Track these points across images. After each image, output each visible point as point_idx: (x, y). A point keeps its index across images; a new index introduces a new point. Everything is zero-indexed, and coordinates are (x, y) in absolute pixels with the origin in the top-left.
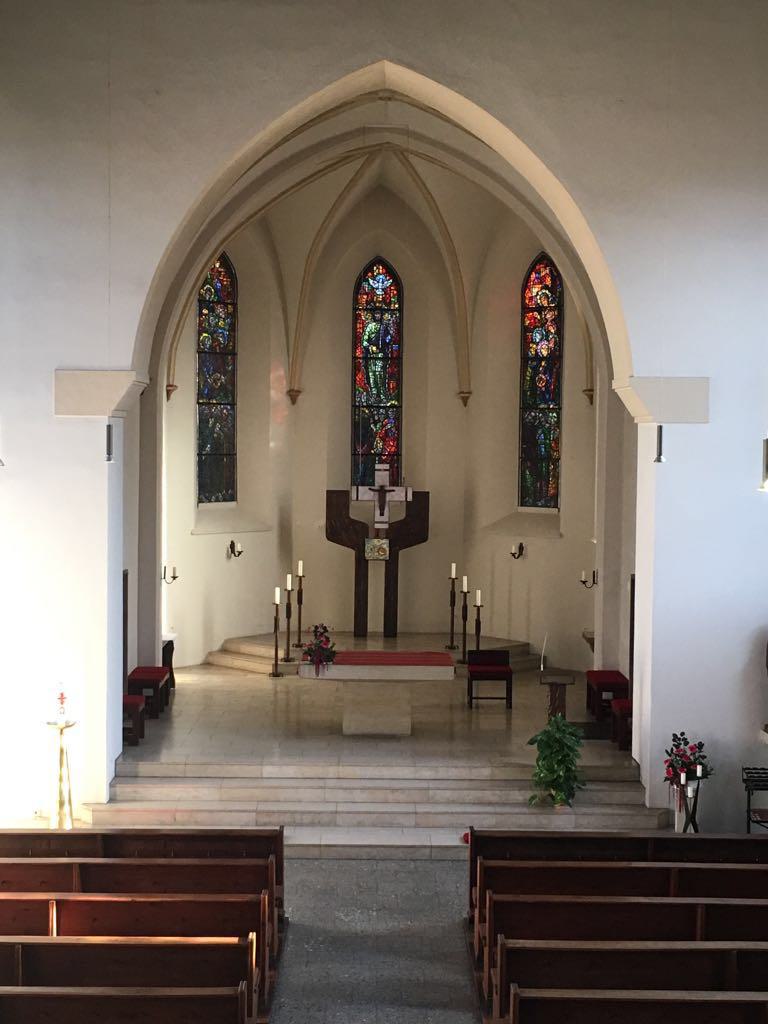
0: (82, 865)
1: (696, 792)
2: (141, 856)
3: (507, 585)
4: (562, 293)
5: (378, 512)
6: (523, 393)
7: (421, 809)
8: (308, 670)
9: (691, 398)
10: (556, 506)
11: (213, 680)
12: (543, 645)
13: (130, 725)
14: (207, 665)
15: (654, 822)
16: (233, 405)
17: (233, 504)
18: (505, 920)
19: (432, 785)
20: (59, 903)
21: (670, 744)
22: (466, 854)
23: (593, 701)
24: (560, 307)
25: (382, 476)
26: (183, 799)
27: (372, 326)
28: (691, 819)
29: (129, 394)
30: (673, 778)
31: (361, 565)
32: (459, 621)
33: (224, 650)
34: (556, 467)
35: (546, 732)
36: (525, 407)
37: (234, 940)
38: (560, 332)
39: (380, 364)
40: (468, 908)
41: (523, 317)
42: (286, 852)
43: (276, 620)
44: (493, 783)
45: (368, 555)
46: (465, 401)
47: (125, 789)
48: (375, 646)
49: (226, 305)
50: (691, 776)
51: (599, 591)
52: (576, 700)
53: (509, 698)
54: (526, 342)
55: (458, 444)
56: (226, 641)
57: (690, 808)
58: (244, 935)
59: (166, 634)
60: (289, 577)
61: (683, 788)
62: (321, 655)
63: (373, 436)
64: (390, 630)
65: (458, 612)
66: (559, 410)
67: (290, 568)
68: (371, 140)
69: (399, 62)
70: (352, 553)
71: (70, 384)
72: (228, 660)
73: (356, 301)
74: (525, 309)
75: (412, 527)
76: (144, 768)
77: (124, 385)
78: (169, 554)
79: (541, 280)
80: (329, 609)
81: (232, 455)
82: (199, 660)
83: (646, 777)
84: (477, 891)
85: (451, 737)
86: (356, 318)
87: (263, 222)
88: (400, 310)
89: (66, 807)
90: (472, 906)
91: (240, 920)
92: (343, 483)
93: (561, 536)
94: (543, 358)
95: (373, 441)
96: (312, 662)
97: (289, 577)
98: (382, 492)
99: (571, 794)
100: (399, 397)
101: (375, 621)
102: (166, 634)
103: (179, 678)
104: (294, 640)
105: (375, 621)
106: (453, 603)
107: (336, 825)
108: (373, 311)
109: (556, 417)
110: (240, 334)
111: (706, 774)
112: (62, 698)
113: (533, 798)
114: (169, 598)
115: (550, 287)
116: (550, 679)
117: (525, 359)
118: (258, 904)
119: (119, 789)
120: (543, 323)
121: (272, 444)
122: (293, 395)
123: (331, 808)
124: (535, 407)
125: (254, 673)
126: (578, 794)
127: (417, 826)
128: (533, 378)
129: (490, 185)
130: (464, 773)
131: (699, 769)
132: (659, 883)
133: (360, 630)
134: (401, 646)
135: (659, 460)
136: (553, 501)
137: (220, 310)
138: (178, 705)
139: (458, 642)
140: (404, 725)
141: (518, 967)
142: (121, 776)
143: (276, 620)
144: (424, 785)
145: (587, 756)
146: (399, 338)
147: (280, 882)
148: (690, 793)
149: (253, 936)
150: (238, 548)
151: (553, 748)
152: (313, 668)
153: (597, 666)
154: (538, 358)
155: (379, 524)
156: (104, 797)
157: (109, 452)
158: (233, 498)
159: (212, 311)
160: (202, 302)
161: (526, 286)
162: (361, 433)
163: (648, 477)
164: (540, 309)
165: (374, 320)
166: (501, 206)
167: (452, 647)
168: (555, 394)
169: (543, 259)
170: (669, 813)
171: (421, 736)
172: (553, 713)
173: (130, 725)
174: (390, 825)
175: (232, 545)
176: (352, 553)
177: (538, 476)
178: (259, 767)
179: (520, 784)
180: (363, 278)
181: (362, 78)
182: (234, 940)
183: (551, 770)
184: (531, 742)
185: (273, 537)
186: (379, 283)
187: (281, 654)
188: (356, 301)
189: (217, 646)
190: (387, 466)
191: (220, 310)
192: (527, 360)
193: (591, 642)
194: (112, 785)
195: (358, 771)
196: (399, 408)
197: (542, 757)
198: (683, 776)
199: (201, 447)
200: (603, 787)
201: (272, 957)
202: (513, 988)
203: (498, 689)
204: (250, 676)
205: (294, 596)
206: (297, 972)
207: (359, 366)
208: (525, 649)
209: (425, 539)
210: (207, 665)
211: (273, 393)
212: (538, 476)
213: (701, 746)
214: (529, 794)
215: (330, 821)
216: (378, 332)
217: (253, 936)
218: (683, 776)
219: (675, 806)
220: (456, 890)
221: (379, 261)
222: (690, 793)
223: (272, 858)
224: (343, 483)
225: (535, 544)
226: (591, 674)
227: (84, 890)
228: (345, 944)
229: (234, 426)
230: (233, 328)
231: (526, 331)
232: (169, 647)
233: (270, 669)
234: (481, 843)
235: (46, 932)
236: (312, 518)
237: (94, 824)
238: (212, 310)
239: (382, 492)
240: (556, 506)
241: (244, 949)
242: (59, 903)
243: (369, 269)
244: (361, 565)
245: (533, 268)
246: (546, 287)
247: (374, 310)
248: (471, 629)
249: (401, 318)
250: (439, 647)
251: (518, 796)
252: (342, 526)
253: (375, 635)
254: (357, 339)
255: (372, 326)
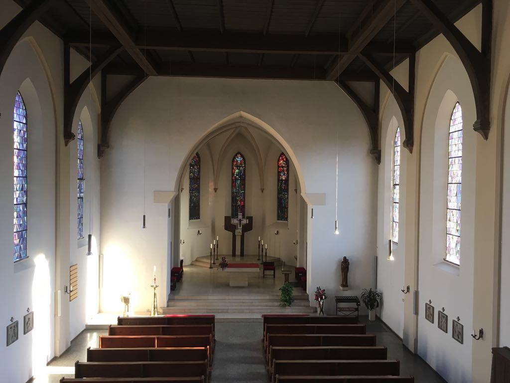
0: (163, 327)
1: (323, 303)
2: (178, 324)
3: (274, 243)
4: (288, 163)
5: (239, 226)
6: (278, 190)
7: (250, 308)
8: (221, 269)
9: (321, 199)
10: (287, 220)
11: (194, 269)
12: (283, 259)
13: (172, 284)
14: (192, 265)
15: (312, 311)
16: (199, 193)
17: (198, 220)
18: (272, 341)
19: (254, 301)
20: (158, 338)
21: (316, 290)
22: (263, 321)
23: (297, 275)
24: (288, 167)
25: (240, 217)
26: (187, 307)
27: (237, 171)
28: (322, 310)
29: (173, 198)
30: (317, 299)
31: (234, 237)
32: (261, 251)
33: (196, 261)
34: (287, 210)
35: (283, 287)
36: (279, 193)
37: (203, 348)
38: (288, 173)
39: (239, 181)
40: (263, 336)
41: (278, 168)
42: (216, 321)
43: (211, 253)
44: (270, 300)
45: (236, 234)
46: (262, 191)
47: (172, 303)
48: (238, 260)
49: (197, 165)
50: (322, 299)
51: (298, 246)
52: (292, 278)
53: (274, 275)
54: (279, 175)
55: (261, 203)
56: (198, 258)
57: (321, 307)
58: (206, 347)
59: (181, 258)
60: (215, 241)
61: (319, 302)
62: (224, 265)
63: (237, 201)
64: (242, 254)
65: (261, 249)
66: (288, 195)
67: (214, 238)
68: (237, 125)
69: (243, 111)
70: (232, 233)
71: (158, 195)
72: (197, 263)
73: (233, 164)
74: (279, 167)
75: (248, 228)
76: (176, 297)
77: (172, 196)
78: (183, 236)
79: (283, 159)
80: (225, 249)
81: (199, 204)
82: (190, 263)
83: (310, 299)
84: (265, 333)
85: (259, 287)
86: (233, 169)
87: (209, 145)
88: (245, 166)
89: (156, 309)
90: (264, 336)
91: (205, 342)
92: (230, 215)
93: (288, 229)
94: (284, 180)
95: (238, 205)
96: (221, 267)
97: (215, 241)
98: (240, 221)
99: (290, 303)
100: (244, 190)
101: (238, 252)
102: (181, 258)
103: (185, 269)
104: (216, 258)
105: (238, 252)
106: (259, 248)
107: (228, 313)
108: (237, 167)
109: (286, 198)
110: (202, 174)
111: (325, 298)
112: (155, 279)
113: (280, 305)
114: (183, 248)
115: (285, 166)
116: (285, 272)
117: (279, 180)
118: (209, 337)
119: (170, 303)
120: (283, 171)
121: (210, 203)
122: (216, 190)
123: (227, 308)
124: (281, 193)
125: (205, 268)
126: (292, 303)
127: (250, 312)
128: (281, 186)
129: (269, 137)
130: (262, 298)
131: (324, 297)
132: (312, 330)
133: (234, 255)
134: (247, 261)
135: (312, 209)
136: (286, 219)
137: (195, 167)
138: (184, 278)
139: (261, 258)
140: (246, 284)
141: (276, 354)
142: (171, 299)
143: (211, 253)
144: (251, 301)
145: (295, 292)
146: (244, 174)
147: (214, 330)
148: (321, 303)
149: (208, 347)
150: (200, 232)
151: (286, 291)
152: (222, 269)
153: (298, 266)
154: (282, 180)
155: (239, 222)
156: (166, 306)
157: (169, 216)
158: (199, 218)
159: (195, 171)
160: (191, 165)
161: (279, 161)
162: (234, 200)
163: (310, 222)
164: (283, 167)
165: (238, 169)
166: (271, 142)
167: (259, 260)
168: (287, 190)
169: (283, 154)
170: (316, 308)
171: (251, 287)
172: (285, 282)
173: (172, 284)
174: (243, 312)
175: (199, 232)
176: (231, 234)
177: (282, 212)
178: (217, 327)
179: (276, 300)
180: (234, 158)
181: (237, 114)
182: (203, 348)
183: (285, 297)
184: (280, 290)
185: (210, 229)
186: (239, 159)
187: (212, 262)
188: (233, 164)
189: (194, 260)
190: (241, 214)
191: (195, 167)
192: (279, 180)
193: (296, 259)
194: (168, 302)
195: (234, 297)
196: (245, 193)
197: (283, 293)
198: (319, 299)
199: (190, 205)
200: (298, 301)
201: (213, 351)
202: (274, 360)
203: (272, 272)
204: (204, 268)
205: (216, 246)
206: (219, 355)
207: (233, 182)
208: (279, 260)
209: (251, 229)
210: (192, 265)
211: (210, 190)
212: (282, 212)
213: (324, 290)
214: (279, 303)
215: (227, 311)
216: (239, 172)
217: (208, 347)
218: (319, 299)
219: (318, 306)
220: (260, 332)
221: (239, 153)
222: (321, 303)
223: (212, 325)
224: (230, 215)
225: (281, 231)
226: (297, 269)
227: (163, 335)
228: (231, 347)
229: (199, 199)
230: (199, 172)
231: (279, 173)
232: (182, 261)
233: (209, 266)
234: (267, 319)
235: (154, 347)
236: (221, 224)
237: (164, 313)
238: (193, 167)
239: (240, 221)
240: (287, 220)
241: (206, 350)
242: (158, 338)
243: (236, 155)
244: (234, 237)
245: (280, 156)
246: (284, 161)
247: (238, 167)
248: (264, 254)
249: (245, 169)
250: (255, 262)
251: (276, 304)
252: (229, 226)
253: (238, 255)
254: (233, 174)
255: (237, 171)
